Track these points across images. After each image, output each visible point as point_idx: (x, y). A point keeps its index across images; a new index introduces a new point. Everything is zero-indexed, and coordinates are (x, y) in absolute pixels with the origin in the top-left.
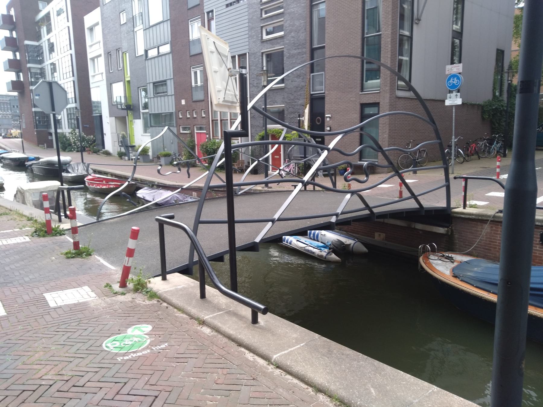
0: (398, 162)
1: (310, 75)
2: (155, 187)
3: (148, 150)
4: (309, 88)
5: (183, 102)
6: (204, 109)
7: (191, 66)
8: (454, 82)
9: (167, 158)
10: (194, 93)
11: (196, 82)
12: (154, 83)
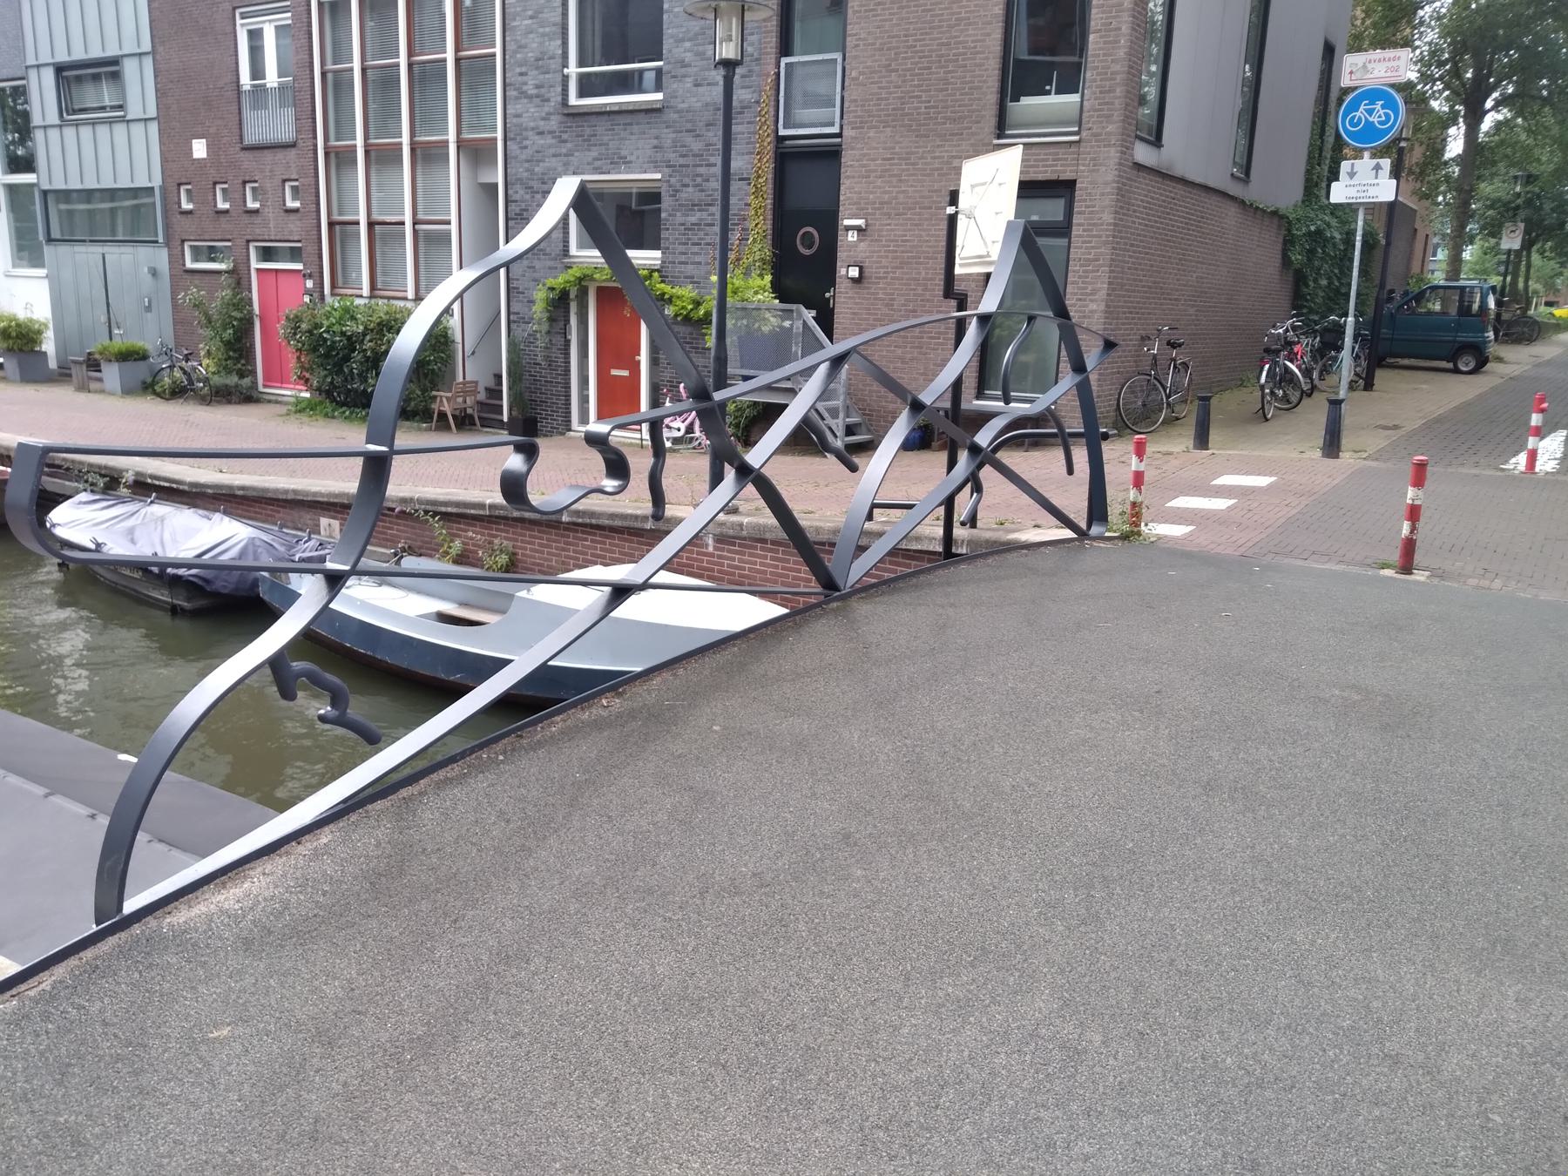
0: (1118, 404)
1: (778, 67)
2: (124, 491)
3: (39, 332)
4: (772, 113)
5: (199, 149)
6: (293, 177)
7: (234, 9)
8: (1374, 119)
9: (129, 365)
10: (247, 114)
11: (257, 71)
12: (60, 69)
